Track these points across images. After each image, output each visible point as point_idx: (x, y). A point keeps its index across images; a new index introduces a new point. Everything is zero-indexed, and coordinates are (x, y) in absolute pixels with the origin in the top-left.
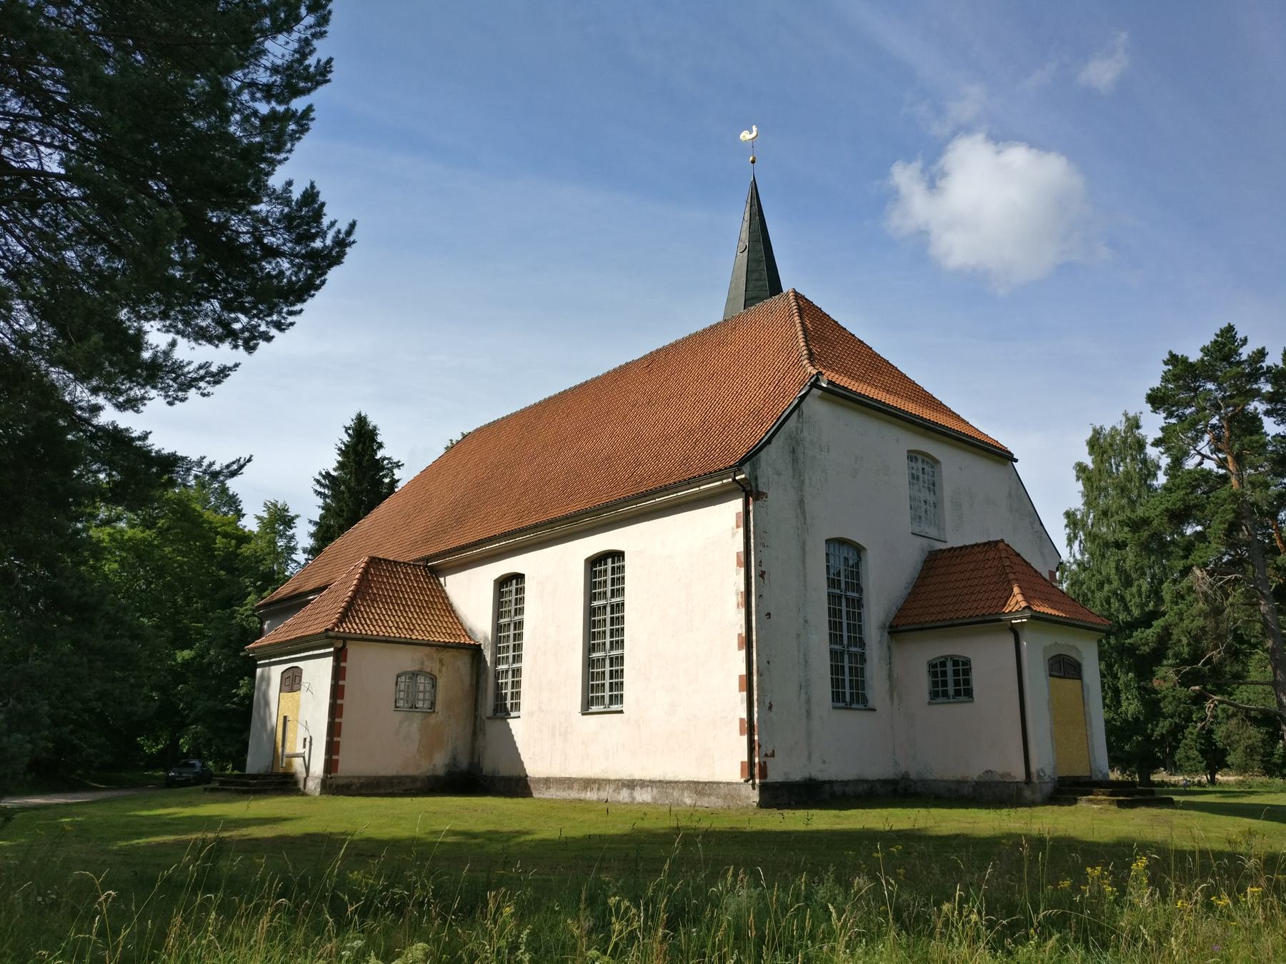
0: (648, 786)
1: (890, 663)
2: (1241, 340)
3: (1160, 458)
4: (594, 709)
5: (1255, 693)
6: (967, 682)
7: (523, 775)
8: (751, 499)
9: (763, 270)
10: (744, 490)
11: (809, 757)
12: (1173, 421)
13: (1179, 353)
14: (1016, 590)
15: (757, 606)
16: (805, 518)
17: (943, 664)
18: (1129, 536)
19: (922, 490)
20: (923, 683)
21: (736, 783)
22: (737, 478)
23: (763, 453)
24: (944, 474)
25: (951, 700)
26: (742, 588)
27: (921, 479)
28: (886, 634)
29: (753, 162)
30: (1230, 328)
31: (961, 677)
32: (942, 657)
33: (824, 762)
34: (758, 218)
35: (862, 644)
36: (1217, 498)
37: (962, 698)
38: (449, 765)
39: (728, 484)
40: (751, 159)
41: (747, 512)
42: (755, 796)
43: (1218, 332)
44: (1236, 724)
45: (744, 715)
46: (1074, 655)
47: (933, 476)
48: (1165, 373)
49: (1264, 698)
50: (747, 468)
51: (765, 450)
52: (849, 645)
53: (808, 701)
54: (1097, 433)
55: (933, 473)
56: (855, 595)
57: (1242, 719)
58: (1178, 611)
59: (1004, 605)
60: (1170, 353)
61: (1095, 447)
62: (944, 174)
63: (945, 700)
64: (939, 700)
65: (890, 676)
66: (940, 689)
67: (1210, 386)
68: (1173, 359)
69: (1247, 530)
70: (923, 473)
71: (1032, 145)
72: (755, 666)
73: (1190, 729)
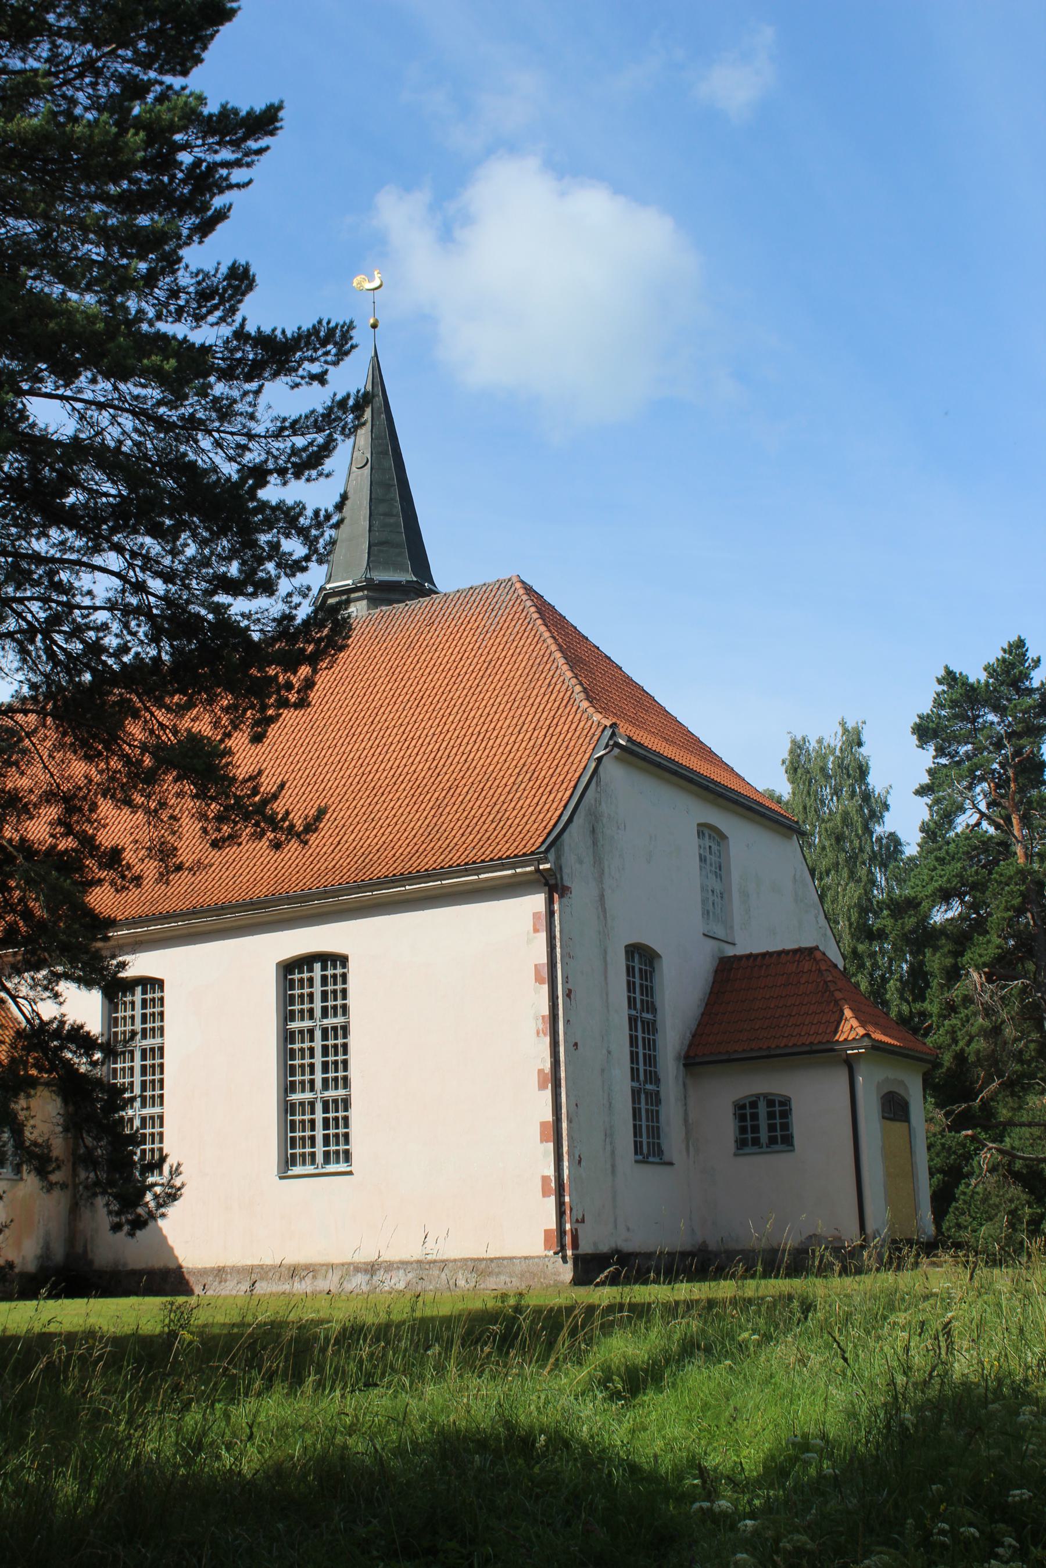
0: (398, 1268)
1: (686, 1104)
2: (1033, 659)
3: (888, 792)
4: (298, 1170)
5: (1020, 1139)
6: (786, 1127)
7: (172, 1266)
8: (556, 896)
9: (393, 499)
10: (546, 884)
11: (616, 1227)
12: (944, 761)
13: (956, 669)
14: (848, 1013)
15: (565, 1033)
16: (605, 917)
17: (754, 1105)
18: (889, 922)
19: (710, 875)
20: (728, 1128)
21: (539, 1257)
22: (541, 867)
23: (566, 835)
24: (731, 854)
25: (764, 1149)
26: (545, 1011)
27: (708, 862)
28: (681, 1067)
29: (374, 326)
30: (1020, 643)
31: (778, 1121)
32: (752, 1095)
33: (628, 1229)
34: (383, 416)
35: (657, 1081)
36: (1001, 875)
37: (779, 1147)
38: (41, 1257)
39: (530, 873)
40: (372, 321)
41: (551, 913)
42: (567, 1272)
43: (1006, 646)
44: (996, 1182)
45: (550, 1172)
46: (902, 1092)
47: (720, 857)
48: (938, 695)
49: (1031, 1145)
50: (551, 856)
51: (568, 830)
52: (645, 1082)
53: (613, 1153)
54: (798, 748)
55: (719, 851)
56: (650, 1016)
57: (1004, 1176)
58: (950, 1029)
59: (836, 1032)
60: (946, 668)
61: (799, 771)
62: (467, 219)
63: (755, 1149)
64: (747, 1150)
65: (686, 1121)
66: (749, 1136)
67: (992, 717)
68: (950, 678)
69: (1033, 918)
70: (710, 853)
71: (618, 188)
72: (564, 1110)
73: (962, 1187)
